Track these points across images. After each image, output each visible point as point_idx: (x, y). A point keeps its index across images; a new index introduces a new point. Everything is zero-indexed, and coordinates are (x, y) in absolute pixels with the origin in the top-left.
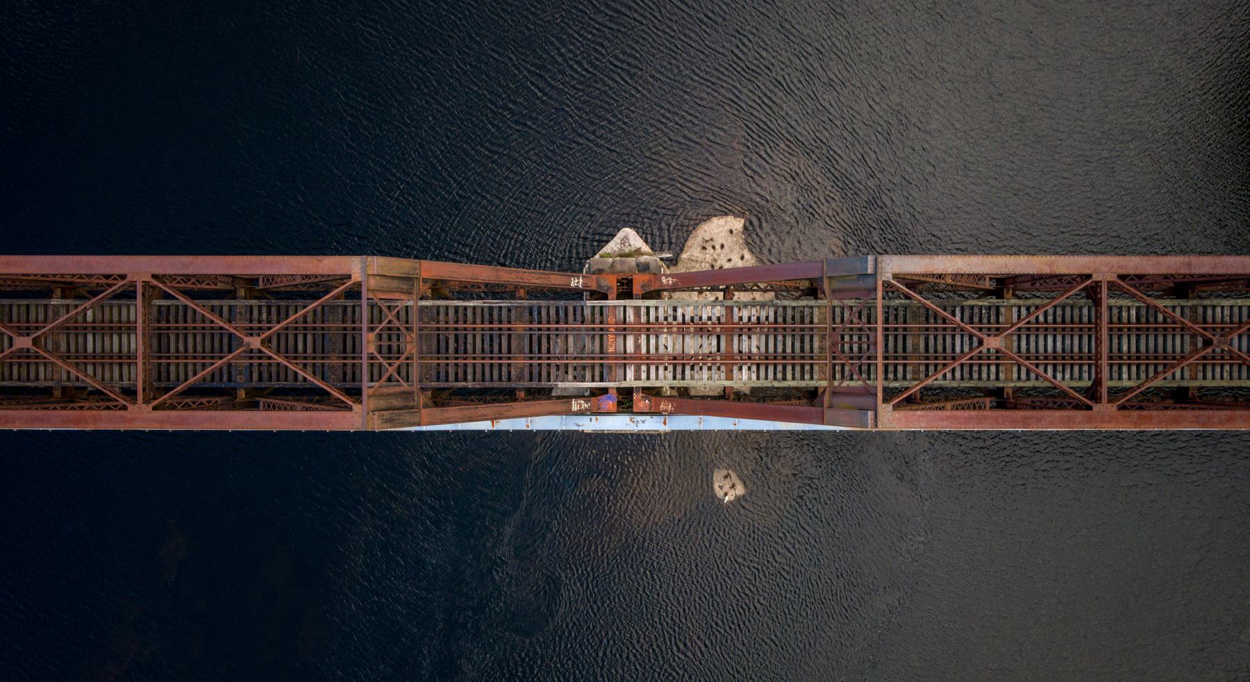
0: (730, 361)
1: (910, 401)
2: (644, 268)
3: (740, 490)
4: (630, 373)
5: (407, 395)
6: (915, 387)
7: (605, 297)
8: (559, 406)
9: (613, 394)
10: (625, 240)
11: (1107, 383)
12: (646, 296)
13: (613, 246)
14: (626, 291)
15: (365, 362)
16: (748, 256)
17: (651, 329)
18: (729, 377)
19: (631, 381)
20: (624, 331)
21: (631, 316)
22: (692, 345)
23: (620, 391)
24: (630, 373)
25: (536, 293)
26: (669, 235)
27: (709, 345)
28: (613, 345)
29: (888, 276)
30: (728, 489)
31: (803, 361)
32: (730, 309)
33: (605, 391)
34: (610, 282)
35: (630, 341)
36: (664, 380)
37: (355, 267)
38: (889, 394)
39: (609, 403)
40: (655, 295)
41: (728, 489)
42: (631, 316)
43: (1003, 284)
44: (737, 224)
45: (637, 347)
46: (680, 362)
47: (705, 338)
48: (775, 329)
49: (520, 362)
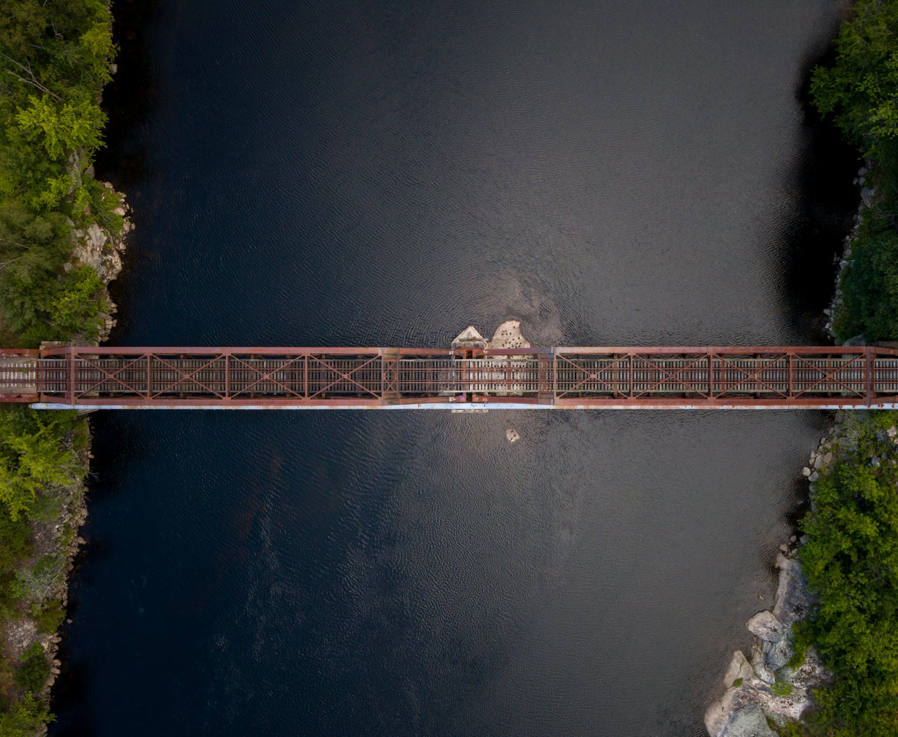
0: (509, 382)
1: (564, 397)
2: (477, 346)
3: (518, 437)
4: (471, 387)
5: (395, 394)
6: (566, 391)
7: (462, 358)
8: (444, 400)
9: (465, 395)
10: (469, 334)
11: (712, 391)
12: (477, 358)
13: (463, 335)
14: (470, 356)
15: (382, 383)
16: (521, 338)
17: (480, 370)
18: (509, 388)
19: (471, 390)
20: (469, 371)
21: (472, 365)
22: (495, 376)
23: (467, 394)
24: (471, 387)
25: (435, 357)
26: (488, 332)
27: (502, 376)
28: (465, 376)
29: (558, 354)
30: (513, 437)
31: (536, 382)
32: (509, 363)
33: (461, 394)
34: (464, 352)
35: (471, 375)
36: (484, 389)
37: (379, 351)
38: (558, 394)
39: (463, 398)
40: (482, 357)
41: (513, 437)
42: (472, 365)
43: (612, 356)
44: (517, 324)
45: (474, 377)
46: (491, 383)
47: (56, 634)
48: (527, 369)
49: (429, 383)
